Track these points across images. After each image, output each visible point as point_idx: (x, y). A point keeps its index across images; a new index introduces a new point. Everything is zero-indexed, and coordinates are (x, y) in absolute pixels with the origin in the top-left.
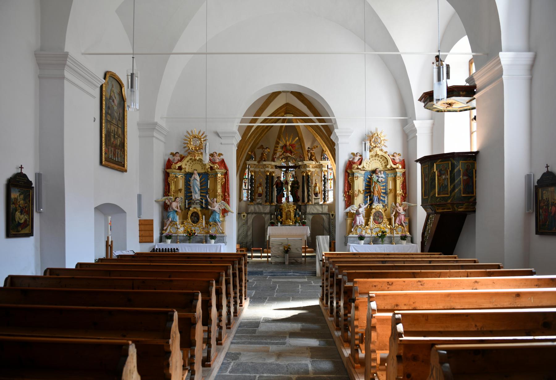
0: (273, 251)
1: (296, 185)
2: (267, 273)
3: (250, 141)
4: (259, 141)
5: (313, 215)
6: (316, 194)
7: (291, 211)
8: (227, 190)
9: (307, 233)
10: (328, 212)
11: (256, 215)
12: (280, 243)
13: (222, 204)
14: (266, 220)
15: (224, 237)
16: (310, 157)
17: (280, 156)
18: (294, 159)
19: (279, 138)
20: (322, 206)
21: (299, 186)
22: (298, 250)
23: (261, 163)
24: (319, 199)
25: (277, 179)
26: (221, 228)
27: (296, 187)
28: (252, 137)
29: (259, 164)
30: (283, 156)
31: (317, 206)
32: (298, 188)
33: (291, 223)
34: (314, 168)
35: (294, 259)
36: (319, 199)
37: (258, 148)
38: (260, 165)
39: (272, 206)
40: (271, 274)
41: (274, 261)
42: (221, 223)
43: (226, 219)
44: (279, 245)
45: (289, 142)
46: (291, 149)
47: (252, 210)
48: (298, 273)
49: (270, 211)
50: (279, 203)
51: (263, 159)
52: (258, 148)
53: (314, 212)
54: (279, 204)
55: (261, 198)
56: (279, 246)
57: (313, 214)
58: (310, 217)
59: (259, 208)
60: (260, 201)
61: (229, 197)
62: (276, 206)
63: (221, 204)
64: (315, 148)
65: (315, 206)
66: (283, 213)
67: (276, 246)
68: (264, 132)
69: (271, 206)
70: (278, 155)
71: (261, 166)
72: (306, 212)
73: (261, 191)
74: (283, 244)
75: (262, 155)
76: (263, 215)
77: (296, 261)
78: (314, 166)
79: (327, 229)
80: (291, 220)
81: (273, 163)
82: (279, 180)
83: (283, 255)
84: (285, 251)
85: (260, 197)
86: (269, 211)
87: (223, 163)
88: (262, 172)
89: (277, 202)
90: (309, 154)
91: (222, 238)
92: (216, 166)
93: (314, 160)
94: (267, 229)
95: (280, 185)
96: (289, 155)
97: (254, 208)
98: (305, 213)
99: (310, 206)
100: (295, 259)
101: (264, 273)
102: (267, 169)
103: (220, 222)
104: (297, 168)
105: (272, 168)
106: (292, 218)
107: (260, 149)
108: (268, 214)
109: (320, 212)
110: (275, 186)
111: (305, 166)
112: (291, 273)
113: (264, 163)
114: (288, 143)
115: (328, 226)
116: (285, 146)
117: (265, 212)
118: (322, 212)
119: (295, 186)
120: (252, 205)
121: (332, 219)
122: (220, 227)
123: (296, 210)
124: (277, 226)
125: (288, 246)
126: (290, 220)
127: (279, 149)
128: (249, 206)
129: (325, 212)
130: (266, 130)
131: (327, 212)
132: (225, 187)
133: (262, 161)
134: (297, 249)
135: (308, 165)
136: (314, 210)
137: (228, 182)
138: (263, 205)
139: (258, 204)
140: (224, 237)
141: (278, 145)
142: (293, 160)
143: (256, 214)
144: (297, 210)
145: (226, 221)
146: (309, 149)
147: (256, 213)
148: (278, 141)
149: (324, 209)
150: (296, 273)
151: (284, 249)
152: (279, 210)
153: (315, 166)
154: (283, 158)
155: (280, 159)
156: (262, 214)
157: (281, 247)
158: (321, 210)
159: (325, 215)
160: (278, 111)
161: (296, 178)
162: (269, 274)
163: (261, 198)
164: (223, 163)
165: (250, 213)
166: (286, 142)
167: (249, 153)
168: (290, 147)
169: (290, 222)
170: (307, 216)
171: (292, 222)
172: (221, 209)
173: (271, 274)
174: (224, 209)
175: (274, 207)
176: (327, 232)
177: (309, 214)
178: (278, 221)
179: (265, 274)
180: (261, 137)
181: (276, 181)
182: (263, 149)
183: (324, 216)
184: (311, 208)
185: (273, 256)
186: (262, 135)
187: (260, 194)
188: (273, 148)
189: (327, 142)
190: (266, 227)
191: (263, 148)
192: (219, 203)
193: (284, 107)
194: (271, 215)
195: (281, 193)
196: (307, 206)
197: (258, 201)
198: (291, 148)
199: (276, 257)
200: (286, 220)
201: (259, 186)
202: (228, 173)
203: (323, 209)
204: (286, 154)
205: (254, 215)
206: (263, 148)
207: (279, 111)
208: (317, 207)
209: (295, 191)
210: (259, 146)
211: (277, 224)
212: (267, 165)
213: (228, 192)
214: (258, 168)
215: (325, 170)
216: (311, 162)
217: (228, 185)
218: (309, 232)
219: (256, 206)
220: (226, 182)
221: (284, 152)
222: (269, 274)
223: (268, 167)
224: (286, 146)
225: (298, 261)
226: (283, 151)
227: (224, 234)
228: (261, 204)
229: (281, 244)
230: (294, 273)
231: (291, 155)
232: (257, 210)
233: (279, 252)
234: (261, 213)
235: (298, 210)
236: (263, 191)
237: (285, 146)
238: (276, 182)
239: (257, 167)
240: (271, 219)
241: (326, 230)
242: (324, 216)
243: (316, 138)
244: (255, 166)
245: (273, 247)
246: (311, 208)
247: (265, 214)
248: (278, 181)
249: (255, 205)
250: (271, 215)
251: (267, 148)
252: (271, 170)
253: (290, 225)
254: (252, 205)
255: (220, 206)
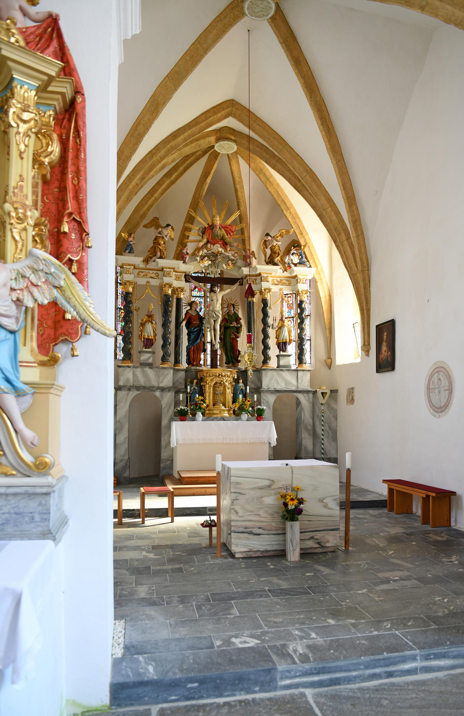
0: (241, 513)
1: (234, 324)
2: (295, 677)
3: (130, 187)
4: (148, 209)
5: (278, 394)
6: (282, 346)
7: (227, 384)
8: (71, 206)
9: (269, 438)
10: (311, 386)
11: (138, 392)
12: (267, 483)
13: (35, 271)
14: (163, 406)
15: (47, 494)
16: (271, 255)
17: (198, 249)
18: (232, 260)
19: (194, 205)
20: (296, 372)
21: (241, 326)
22: (326, 506)
23: (152, 265)
24: (290, 356)
25: (189, 308)
26: (28, 434)
27: (234, 326)
28: (138, 177)
29: (148, 266)
30: (205, 251)
31: (286, 372)
32: (238, 330)
33: (226, 412)
34: (277, 285)
35: (312, 538)
36: (290, 356)
37: (145, 226)
38: (150, 269)
39: (179, 370)
40: (316, 678)
41: (246, 550)
42: (28, 399)
43: (61, 380)
44: (261, 488)
45: (220, 217)
46: (223, 235)
47: (128, 380)
48: (443, 656)
49: (173, 384)
50: (193, 365)
51: (159, 254)
52: (145, 226)
53: (279, 388)
54: (193, 368)
55: (150, 350)
56: (258, 493)
57: (277, 391)
58: (271, 399)
59: (146, 376)
60: (149, 358)
61: (85, 247)
62: (186, 371)
63: (28, 273)
64: (282, 237)
65: (281, 372)
66: (207, 389)
67: (252, 492)
68: (162, 188)
69: (176, 371)
70: (190, 248)
71: (151, 272)
72: (260, 387)
73: (152, 335)
74: (274, 487)
75: (154, 243)
76: (158, 394)
77: (319, 543)
78: (277, 281)
79: (310, 428)
80: (227, 406)
81: (183, 267)
82: (193, 309)
83: (274, 524)
84: (288, 511)
85: (149, 348)
86: (170, 384)
87: (55, 44)
88: (152, 287)
89: (189, 362)
90: (268, 252)
91: (33, 505)
92: (22, 194)
93: (280, 264)
94: (169, 428)
95: (196, 322)
96: (220, 249)
97: (134, 375)
98: (258, 390)
99: (270, 373)
100: (318, 535)
101: (282, 678)
102: (166, 280)
103: (19, 393)
104: (238, 284)
105: (178, 278)
106: (229, 402)
107: (151, 227)
108: (169, 391)
109: (293, 388)
110: (184, 323)
111: (256, 280)
112: (414, 658)
113: (162, 263)
114: (218, 219)
115: (311, 421)
116: (212, 227)
117: (161, 385)
118: (298, 387)
119: (231, 325)
120: (129, 367)
121: (322, 404)
122: (21, 425)
123: (236, 381)
124: (194, 420)
125: (293, 490)
126: (224, 405)
127: (194, 235)
128: (121, 369)
129: (304, 388)
130: (168, 182)
131: (310, 389)
132: (63, 190)
133: (153, 259)
134: (321, 500)
135: (265, 275)
136: (278, 383)
137: (77, 157)
138: (157, 367)
139: (144, 365)
140: (47, 494)
141: (190, 226)
142: (230, 262)
143: (138, 390)
144: (239, 383)
145: (62, 388)
146: (269, 238)
147: (138, 388)
148: (193, 214)
149: (302, 380)
150: (438, 657)
151: (285, 504)
152: (195, 381)
153: (279, 279)
154: (204, 257)
155: (198, 258)
156: (154, 391)
157: (270, 495)
158: (294, 382)
159: (305, 395)
160: (207, 118)
161: (234, 308)
162: (305, 679)
163: (150, 350)
164: (55, 44)
165: (124, 386)
166: (213, 217)
167: (123, 235)
168: (223, 230)
169: (224, 410)
170: (264, 398)
171: (229, 411)
172: (30, 303)
173: (316, 678)
174: (54, 304)
175: (182, 374)
176: (310, 434)
177: (269, 391)
178: (196, 407)
179: (288, 682)
180: (153, 198)
181: (187, 312)
182: (157, 229)
183: (301, 397)
184: (271, 379)
185: (241, 530)
186: (156, 195)
187: (148, 339)
188: (179, 229)
189: (330, 209)
190: (164, 422)
191: (158, 226)
192: (18, 266)
193: (223, 109)
194: (177, 392)
195: (199, 340)
196: (264, 372)
197: (144, 357)
198: (225, 234)
199: (251, 533)
200: (214, 405)
201: (146, 322)
202: (78, 107)
203: (299, 380)
204: (212, 246)
205: (134, 393)
206: (158, 226)
207: (210, 117)
208: (286, 375)
209: (233, 336)
210: (147, 220)
211: (194, 415)
212: (168, 270)
213: (80, 213)
214: (143, 276)
215: (304, 289)
216: (271, 267)
217: (78, 173)
218: (274, 436)
219: (138, 371)
220: (71, 155)
221: (208, 242)
222: (305, 679)
223: (169, 275)
224: (212, 229)
225: (328, 545)
226: (205, 240)
227: (46, 474)
228: (150, 365)
229: (269, 486)
230: (427, 658)
231: (225, 249)
232: (142, 381)
233: (261, 513)
234: (152, 389)
235: (241, 381)
236: (155, 335)
237: (212, 227)
238: (186, 314)
239: (142, 274)
240: (177, 404)
241: (306, 428)
242: (301, 397)
243: (284, 211)
244: (137, 271)
245: (240, 497)
246: (271, 379)
247: (163, 389)
248: (190, 312)
249: (137, 367)
250: (177, 392)
251: (168, 225)
252: (176, 284)
253: (223, 419)
254: (129, 367)
255: (23, 284)
